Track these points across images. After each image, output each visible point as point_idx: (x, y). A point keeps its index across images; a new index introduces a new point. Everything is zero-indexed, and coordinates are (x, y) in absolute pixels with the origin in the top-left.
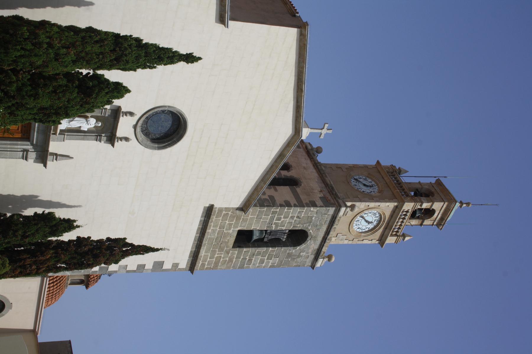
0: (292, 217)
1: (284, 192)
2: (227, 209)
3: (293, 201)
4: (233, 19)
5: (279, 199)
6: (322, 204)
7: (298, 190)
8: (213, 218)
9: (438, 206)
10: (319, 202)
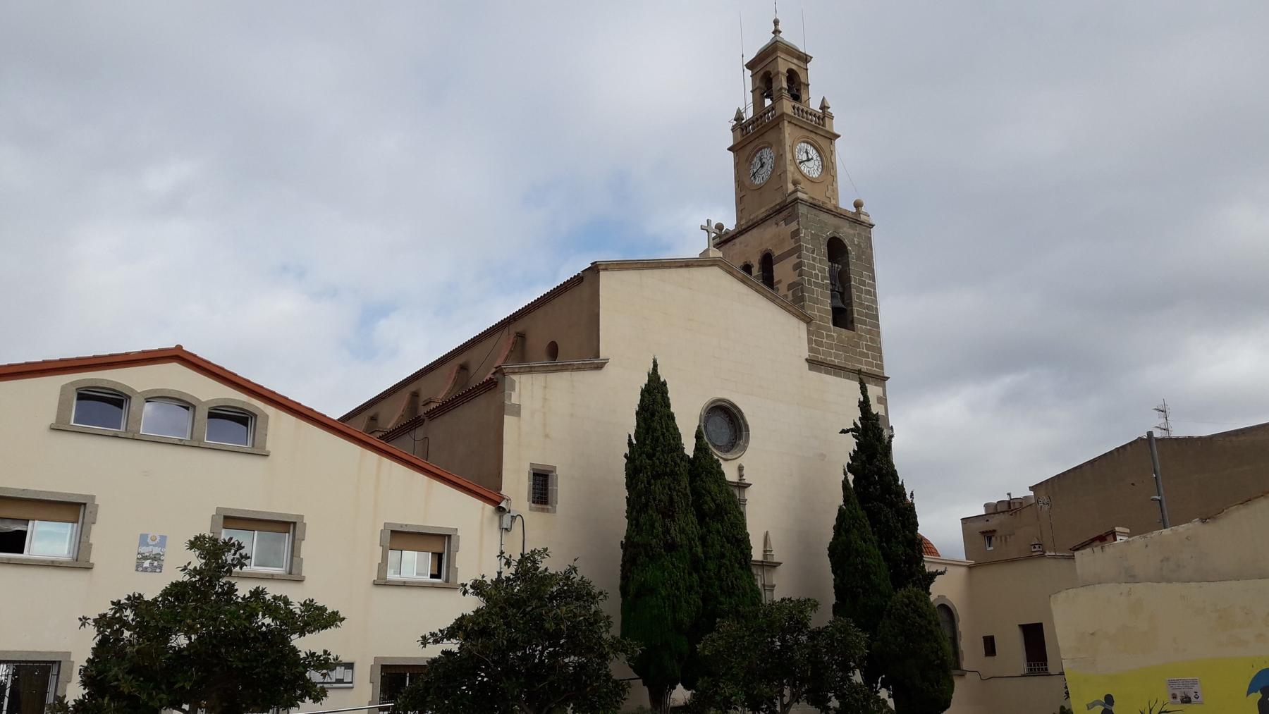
0: (814, 259)
1: (783, 272)
2: (810, 341)
3: (794, 259)
4: (597, 356)
5: (793, 277)
6: (795, 223)
7: (777, 253)
8: (821, 357)
9: (783, 64)
10: (793, 226)
